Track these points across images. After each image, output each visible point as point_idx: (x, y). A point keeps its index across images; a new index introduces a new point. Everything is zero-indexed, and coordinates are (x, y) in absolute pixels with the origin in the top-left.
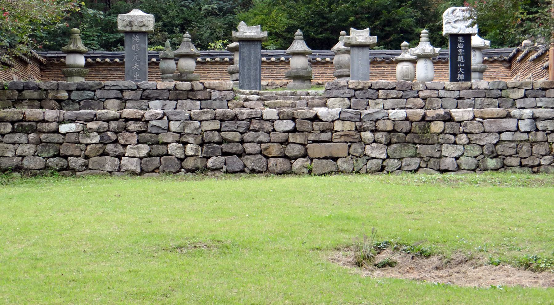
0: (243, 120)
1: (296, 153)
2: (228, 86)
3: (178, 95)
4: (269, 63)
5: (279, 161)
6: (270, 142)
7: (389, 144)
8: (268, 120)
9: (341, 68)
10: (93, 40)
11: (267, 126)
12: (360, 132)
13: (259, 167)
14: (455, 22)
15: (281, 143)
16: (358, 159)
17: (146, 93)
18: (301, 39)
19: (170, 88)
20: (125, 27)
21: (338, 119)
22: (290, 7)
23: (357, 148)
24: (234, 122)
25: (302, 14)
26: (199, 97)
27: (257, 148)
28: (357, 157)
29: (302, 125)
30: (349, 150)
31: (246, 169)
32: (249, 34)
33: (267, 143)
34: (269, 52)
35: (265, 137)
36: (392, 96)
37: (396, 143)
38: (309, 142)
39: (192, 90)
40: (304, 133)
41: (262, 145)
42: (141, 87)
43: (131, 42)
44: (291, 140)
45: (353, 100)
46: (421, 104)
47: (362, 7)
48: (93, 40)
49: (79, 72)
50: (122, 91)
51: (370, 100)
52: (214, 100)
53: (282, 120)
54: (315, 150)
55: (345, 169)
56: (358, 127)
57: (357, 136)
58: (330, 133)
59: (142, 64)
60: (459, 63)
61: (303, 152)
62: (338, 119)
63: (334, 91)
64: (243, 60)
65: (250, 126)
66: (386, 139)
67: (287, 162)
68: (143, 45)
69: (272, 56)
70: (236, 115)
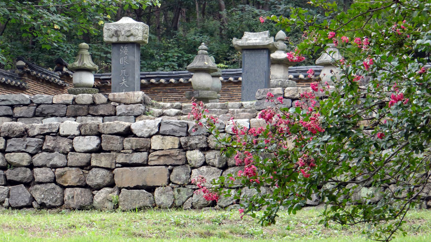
0: (34, 137)
1: (99, 181)
2: (135, 98)
3: (76, 110)
5: (76, 192)
6: (67, 166)
7: (225, 168)
8: (66, 136)
10: (173, 61)
11: (64, 144)
12: (186, 151)
13: (50, 200)
15: (82, 167)
16: (181, 188)
17: (39, 109)
20: (111, 37)
21: (157, 133)
23: (179, 174)
24: (22, 139)
26: (101, 112)
27: (48, 174)
28: (180, 186)
29: (108, 143)
30: (169, 175)
31: (34, 203)
32: (254, 41)
33: (64, 167)
35: (60, 159)
37: (234, 166)
38: (117, 165)
40: (112, 153)
41: (57, 170)
42: (34, 101)
43: (119, 54)
44: (94, 163)
48: (173, 61)
50: (12, 107)
52: (120, 115)
53: (85, 135)
54: (124, 176)
55: (162, 203)
56: (182, 144)
57: (180, 157)
58: (146, 153)
59: (130, 79)
61: (108, 179)
62: (157, 133)
64: (246, 72)
65: (43, 144)
66: (220, 161)
67: (86, 192)
68: (131, 58)
70: (26, 130)
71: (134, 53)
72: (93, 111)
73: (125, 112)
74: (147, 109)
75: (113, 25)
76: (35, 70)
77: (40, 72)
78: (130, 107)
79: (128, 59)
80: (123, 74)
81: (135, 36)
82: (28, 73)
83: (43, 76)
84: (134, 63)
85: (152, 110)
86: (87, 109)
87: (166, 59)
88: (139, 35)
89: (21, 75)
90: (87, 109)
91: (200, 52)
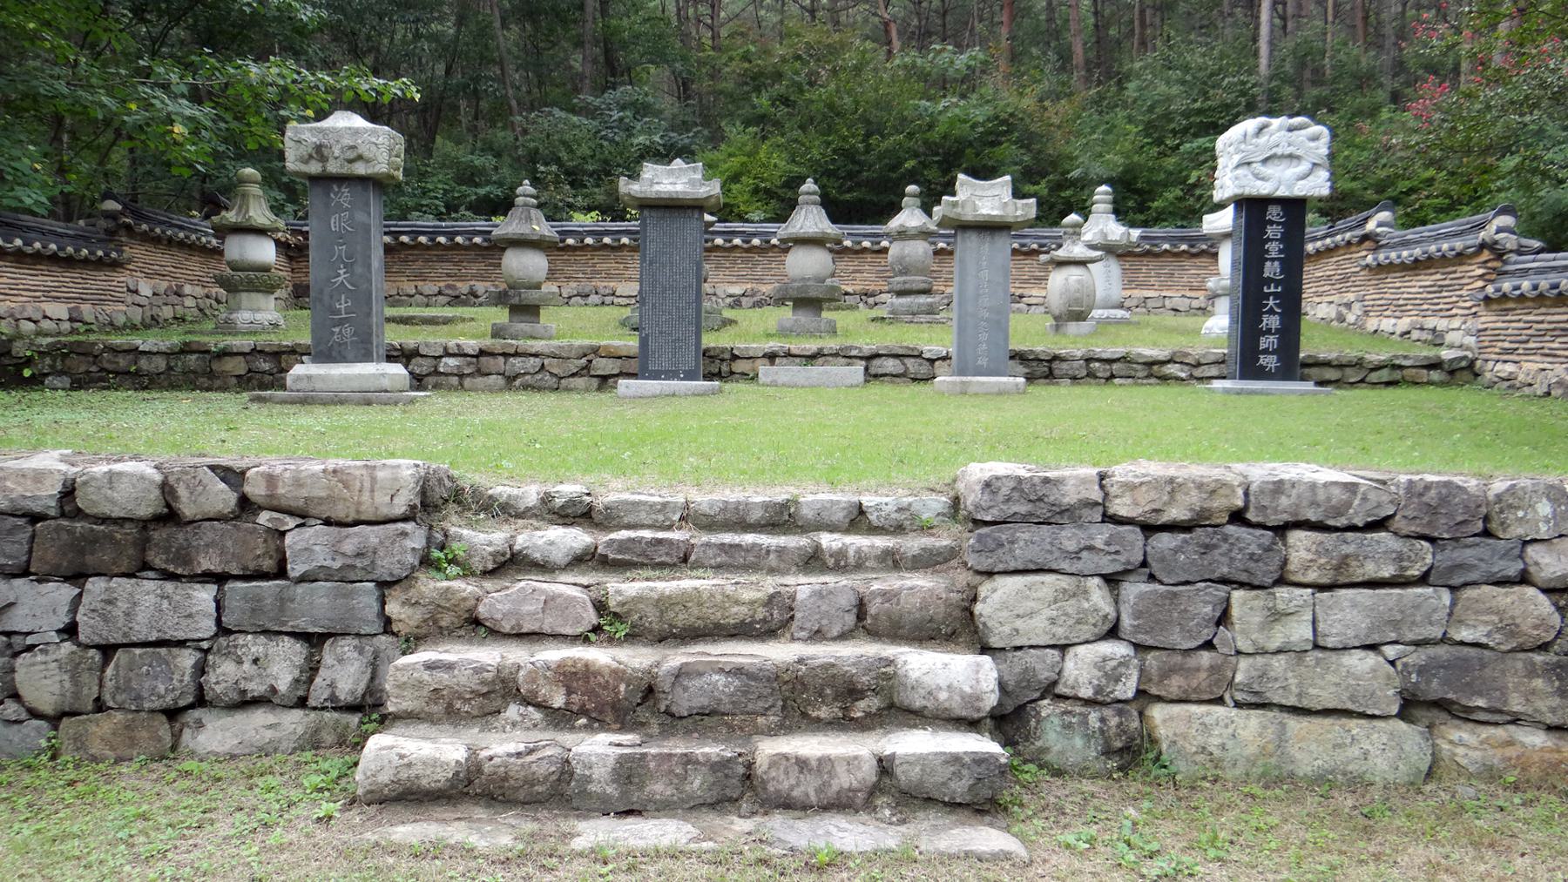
2: (382, 499)
4: (748, 250)
9: (906, 274)
14: (1265, 161)
18: (814, 203)
19: (36, 507)
20: (306, 162)
22: (796, 141)
25: (815, 154)
26: (207, 563)
32: (670, 188)
34: (748, 228)
36: (1370, 570)
39: (169, 516)
43: (327, 205)
45: (1134, 589)
46: (1542, 623)
47: (926, 142)
49: (250, 281)
51: (1238, 595)
52: (303, 579)
59: (359, 270)
60: (1269, 281)
63: (1024, 534)
64: (651, 264)
68: (360, 216)
69: (754, 235)
71: (367, 204)
72: (167, 550)
73: (328, 563)
74: (439, 537)
75: (311, 130)
76: (147, 219)
77: (161, 223)
78: (353, 539)
79: (351, 217)
80: (340, 256)
81: (368, 161)
82: (128, 227)
83: (181, 235)
84: (367, 229)
85: (460, 538)
86: (135, 544)
87: (424, 193)
88: (380, 159)
89: (111, 233)
90: (135, 544)
91: (519, 201)
